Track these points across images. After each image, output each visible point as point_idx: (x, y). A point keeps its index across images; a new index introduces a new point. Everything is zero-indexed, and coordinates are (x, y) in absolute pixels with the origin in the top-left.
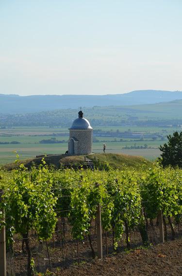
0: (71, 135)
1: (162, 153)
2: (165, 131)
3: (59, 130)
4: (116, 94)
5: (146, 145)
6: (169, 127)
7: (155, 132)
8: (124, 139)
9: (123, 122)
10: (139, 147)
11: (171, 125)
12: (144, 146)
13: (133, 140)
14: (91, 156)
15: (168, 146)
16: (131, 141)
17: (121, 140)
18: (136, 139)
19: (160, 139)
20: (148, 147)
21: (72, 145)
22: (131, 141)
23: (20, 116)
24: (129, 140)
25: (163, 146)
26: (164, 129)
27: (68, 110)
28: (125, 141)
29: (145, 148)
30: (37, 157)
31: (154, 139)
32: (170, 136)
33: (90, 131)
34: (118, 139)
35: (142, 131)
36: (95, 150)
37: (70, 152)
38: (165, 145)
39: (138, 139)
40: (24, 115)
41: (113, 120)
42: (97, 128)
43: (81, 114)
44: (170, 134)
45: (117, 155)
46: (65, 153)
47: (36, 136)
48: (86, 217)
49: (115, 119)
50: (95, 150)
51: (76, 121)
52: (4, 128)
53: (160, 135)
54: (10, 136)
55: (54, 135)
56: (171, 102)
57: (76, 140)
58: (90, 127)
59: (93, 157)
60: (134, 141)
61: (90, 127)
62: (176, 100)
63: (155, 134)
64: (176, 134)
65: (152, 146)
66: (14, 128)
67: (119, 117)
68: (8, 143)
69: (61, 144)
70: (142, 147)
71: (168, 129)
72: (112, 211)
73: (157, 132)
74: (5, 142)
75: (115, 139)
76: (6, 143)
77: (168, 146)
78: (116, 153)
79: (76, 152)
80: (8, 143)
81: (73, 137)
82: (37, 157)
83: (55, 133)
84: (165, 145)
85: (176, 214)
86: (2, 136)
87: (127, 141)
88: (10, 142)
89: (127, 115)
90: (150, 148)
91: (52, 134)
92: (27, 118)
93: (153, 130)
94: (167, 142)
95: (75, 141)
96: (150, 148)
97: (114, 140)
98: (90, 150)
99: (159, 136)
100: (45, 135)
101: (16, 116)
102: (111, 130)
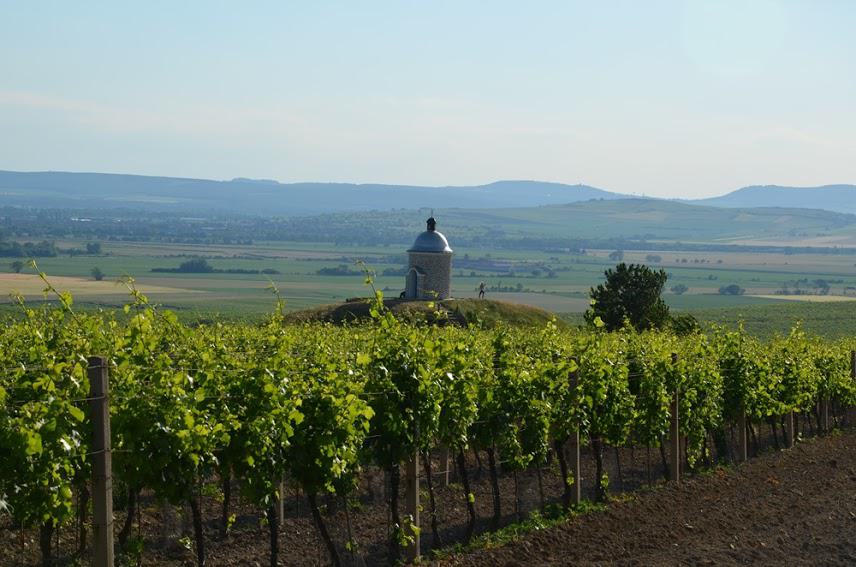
0: (412, 263)
1: (593, 302)
2: (557, 259)
3: (353, 250)
4: (463, 185)
5: (519, 285)
6: (563, 252)
7: (536, 261)
8: (478, 273)
9: (476, 240)
10: (506, 288)
11: (567, 250)
12: (515, 287)
13: (496, 274)
14: (449, 302)
15: (605, 288)
16: (492, 276)
17: (473, 275)
18: (501, 274)
19: (546, 274)
20: (525, 287)
21: (413, 281)
22: (492, 276)
23: (280, 221)
24: (488, 274)
25: (595, 289)
26: (554, 255)
27: (371, 212)
28: (519, 277)
29: (517, 291)
30: (347, 300)
31: (536, 273)
32: (610, 270)
33: (448, 255)
34: (467, 272)
35: (513, 258)
36: (461, 290)
37: (409, 294)
38: (600, 287)
39: (504, 274)
40: (288, 220)
41: (457, 236)
42: (461, 253)
43: (431, 223)
44: (611, 267)
45: (498, 304)
46: (398, 296)
47: (309, 260)
48: (664, 411)
49: (461, 233)
50: (461, 290)
51: (423, 237)
52: (250, 243)
53: (546, 266)
54: (260, 258)
55: (345, 260)
56: (569, 205)
57: (422, 272)
58: (448, 249)
59: (453, 306)
60: (499, 276)
61: (448, 249)
62: (579, 202)
63: (537, 265)
64: (621, 268)
65: (532, 288)
66: (268, 245)
67: (469, 230)
68: (257, 272)
69: (358, 277)
70: (511, 290)
71: (562, 257)
72: (535, 418)
73: (542, 261)
74: (251, 269)
75: (461, 272)
76: (252, 272)
77: (605, 288)
78: (495, 300)
79: (420, 295)
80: (257, 272)
81: (417, 267)
82: (347, 300)
83: (347, 256)
84: (600, 287)
85: (769, 414)
86: (246, 258)
87: (483, 276)
88: (261, 270)
89: (484, 227)
90: (527, 291)
91: (340, 257)
92: (294, 225)
93: (381, 250)
94: (604, 282)
95: (418, 275)
96: (527, 291)
97: (459, 274)
98: (447, 291)
99: (546, 270)
100: (328, 260)
101: (272, 221)
102: (488, 255)
